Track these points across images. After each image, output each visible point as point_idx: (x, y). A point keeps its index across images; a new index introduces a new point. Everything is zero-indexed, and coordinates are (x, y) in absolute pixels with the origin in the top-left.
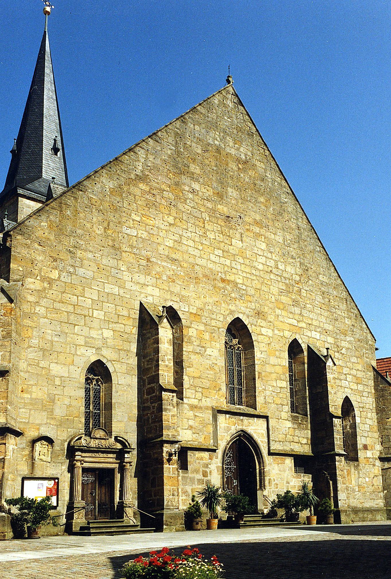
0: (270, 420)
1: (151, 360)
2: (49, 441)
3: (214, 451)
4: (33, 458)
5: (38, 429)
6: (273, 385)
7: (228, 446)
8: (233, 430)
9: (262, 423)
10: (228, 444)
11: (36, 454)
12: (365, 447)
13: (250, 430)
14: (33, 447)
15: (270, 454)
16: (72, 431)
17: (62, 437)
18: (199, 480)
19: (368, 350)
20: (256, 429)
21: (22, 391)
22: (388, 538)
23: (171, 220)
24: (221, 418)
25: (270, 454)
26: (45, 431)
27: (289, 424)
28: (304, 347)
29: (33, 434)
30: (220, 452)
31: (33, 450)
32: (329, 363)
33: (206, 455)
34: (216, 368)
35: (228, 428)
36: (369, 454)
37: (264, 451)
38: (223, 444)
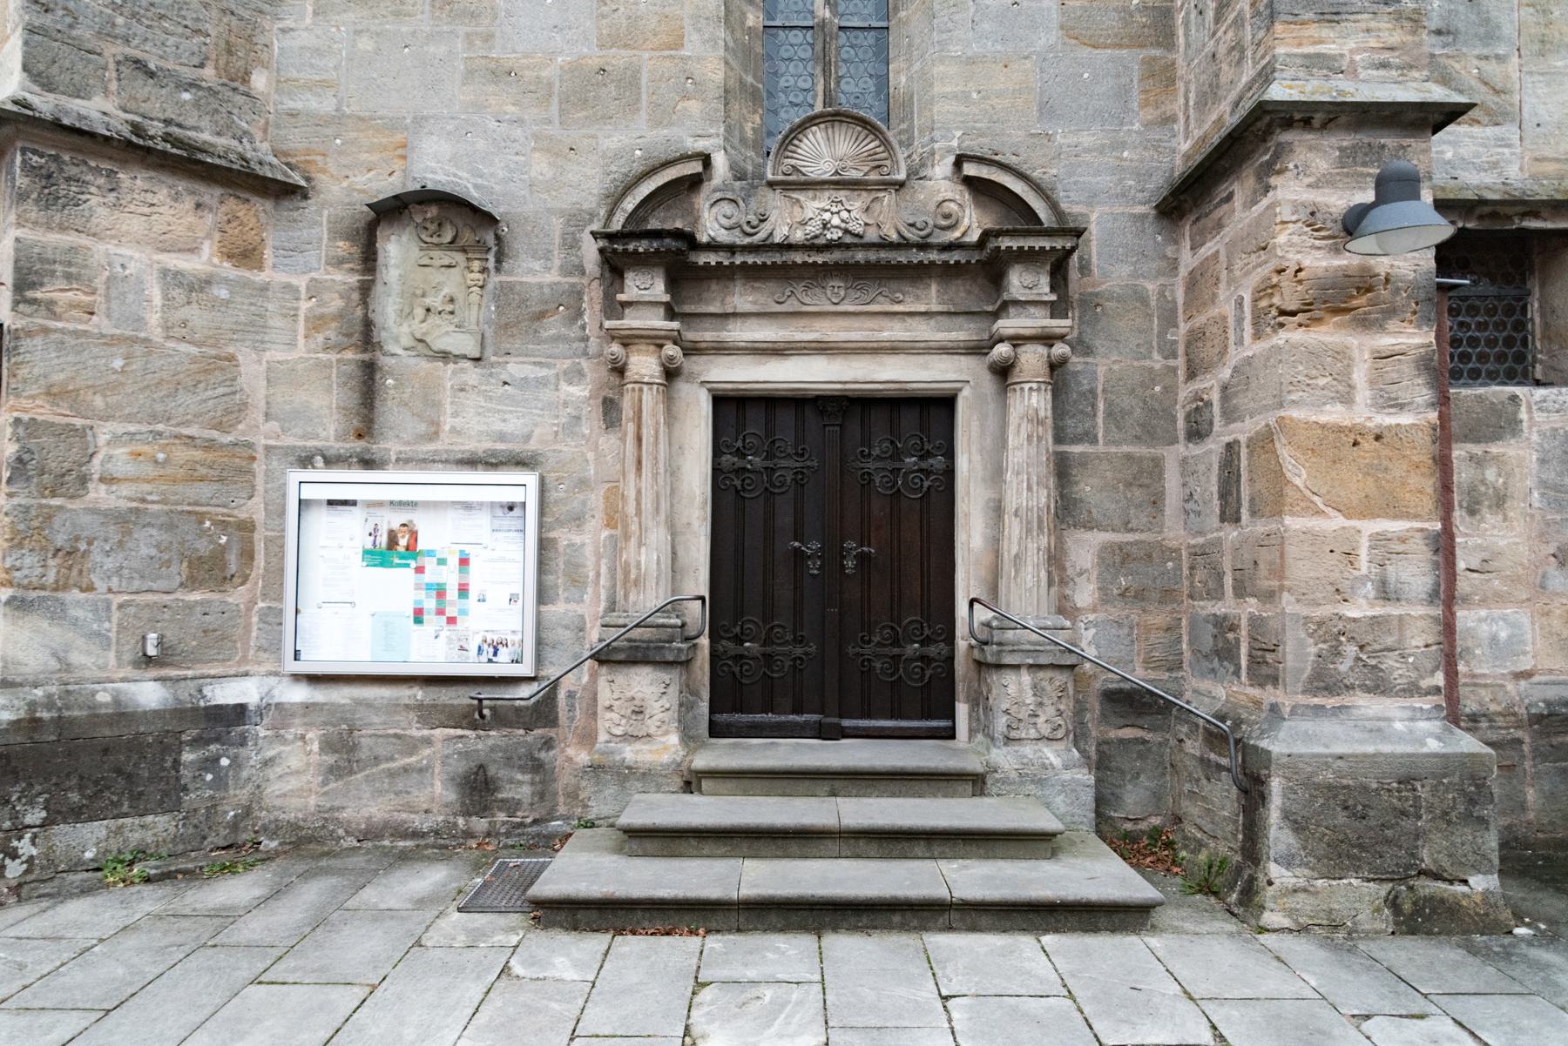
2: (457, 219)
4: (367, 335)
5: (403, 151)
11: (388, 308)
14: (369, 259)
17: (552, 183)
22: (846, 723)
26: (436, 165)
29: (351, 181)
31: (366, 290)
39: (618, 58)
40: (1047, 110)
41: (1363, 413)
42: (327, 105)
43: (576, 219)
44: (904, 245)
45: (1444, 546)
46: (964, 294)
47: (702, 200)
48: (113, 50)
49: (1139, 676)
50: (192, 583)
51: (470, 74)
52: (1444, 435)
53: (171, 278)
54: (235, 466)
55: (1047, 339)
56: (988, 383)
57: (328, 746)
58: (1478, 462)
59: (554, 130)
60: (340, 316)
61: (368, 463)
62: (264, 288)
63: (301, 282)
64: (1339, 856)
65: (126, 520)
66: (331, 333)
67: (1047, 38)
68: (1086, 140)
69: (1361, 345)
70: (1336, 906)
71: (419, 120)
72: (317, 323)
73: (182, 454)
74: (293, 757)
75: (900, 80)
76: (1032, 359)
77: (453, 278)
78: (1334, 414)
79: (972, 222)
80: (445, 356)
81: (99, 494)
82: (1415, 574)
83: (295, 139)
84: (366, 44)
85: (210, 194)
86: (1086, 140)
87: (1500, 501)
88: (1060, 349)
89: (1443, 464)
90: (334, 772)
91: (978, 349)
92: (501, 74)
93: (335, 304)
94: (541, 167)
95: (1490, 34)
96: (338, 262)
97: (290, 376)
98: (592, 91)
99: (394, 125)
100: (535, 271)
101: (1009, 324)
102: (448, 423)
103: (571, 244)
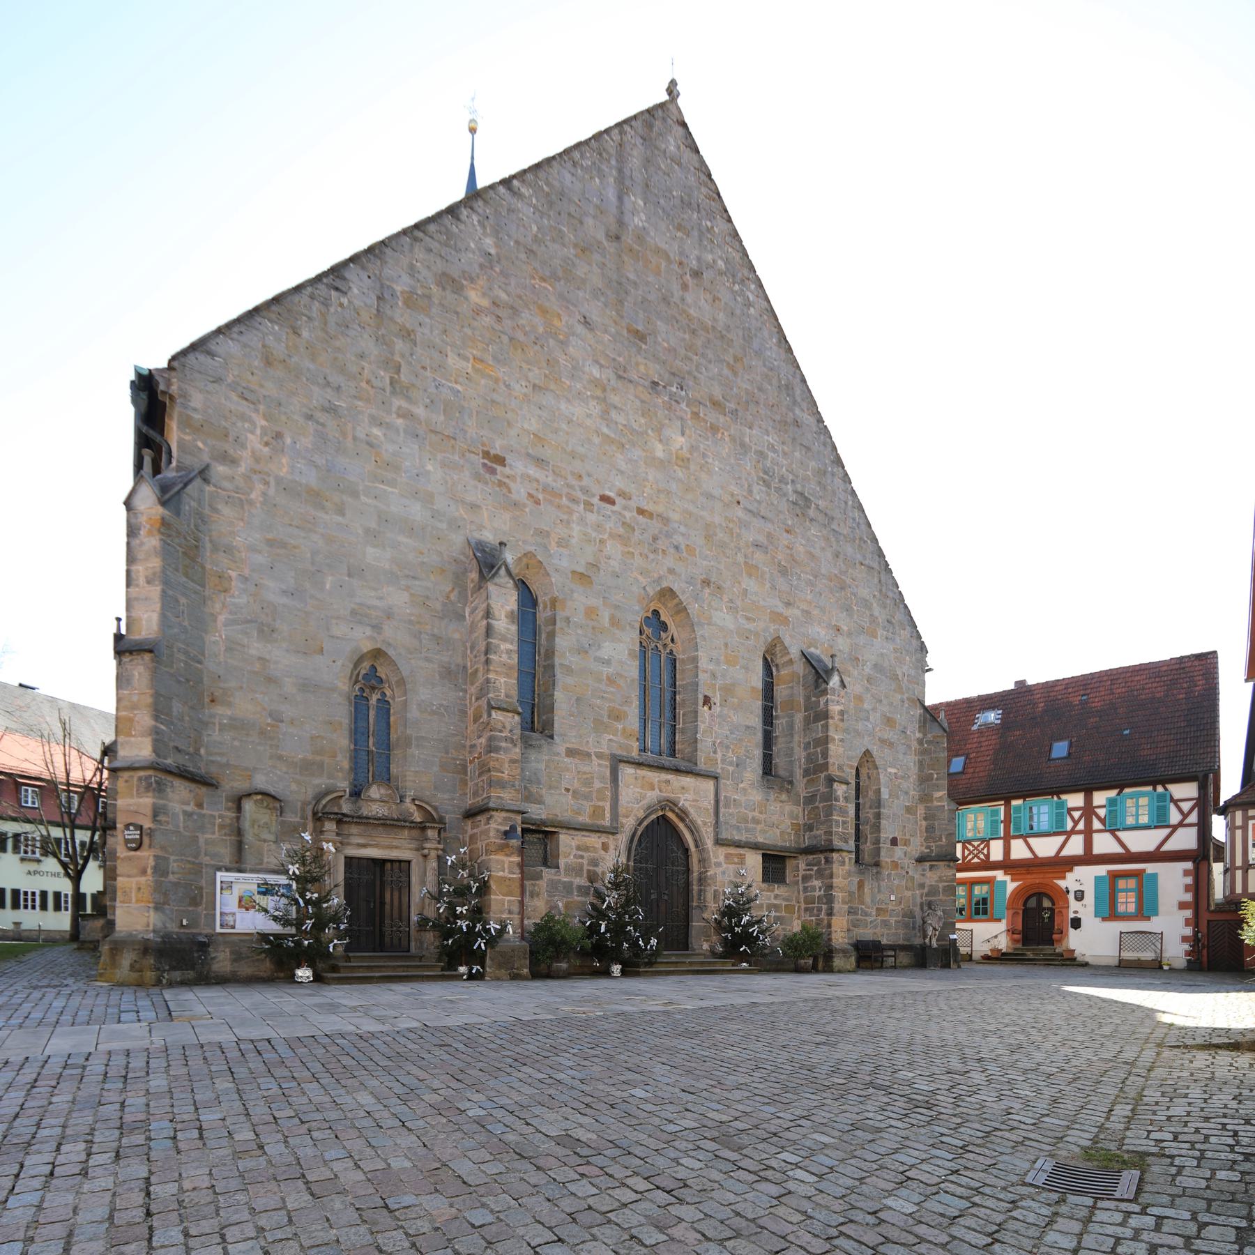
0: (722, 781)
1: (622, 133)
3: (613, 834)
4: (239, 832)
5: (250, 777)
6: (726, 727)
7: (641, 829)
8: (652, 796)
9: (710, 785)
10: (640, 824)
12: (894, 842)
13: (685, 801)
14: (239, 809)
15: (719, 842)
16: (321, 782)
18: (580, 888)
19: (545, 281)
20: (692, 795)
21: (212, 701)
23: (535, 375)
24: (627, 772)
25: (719, 842)
26: (260, 782)
27: (756, 796)
28: (794, 652)
30: (623, 839)
31: (238, 818)
32: (834, 681)
33: (594, 840)
34: (621, 682)
35: (639, 793)
36: (899, 851)
37: (709, 843)
38: (629, 823)
39: (318, 758)
40: (436, 788)
41: (506, 874)
42: (224, 760)
43: (305, 804)
44: (398, 820)
45: (522, 903)
46: (415, 833)
47: (342, 801)
48: (172, 744)
49: (470, 801)
50: (190, 905)
51: (271, 757)
52: (522, 879)
53: (185, 812)
54: (197, 870)
55: (437, 849)
56: (421, 859)
57: (232, 953)
58: (534, 885)
59: (298, 777)
60: (231, 825)
61: (240, 871)
62: (204, 815)
63: (216, 814)
64: (500, 966)
65: (176, 884)
66: (227, 831)
67: (436, 769)
68: (446, 796)
69: (507, 859)
70: (288, 441)
71: (255, 769)
72: (222, 827)
73: (188, 866)
74: (221, 956)
75: (394, 770)
76: (433, 854)
77: (264, 816)
78: (501, 874)
79: (417, 817)
80: (265, 841)
81: (171, 877)
82: (516, 908)
83: (214, 770)
84: (236, 743)
85: (193, 786)
86: (446, 796)
87: (538, 895)
88: (440, 852)
89: (522, 886)
90: (235, 960)
91: (417, 850)
92: (280, 758)
93: (228, 821)
94: (294, 787)
95: (539, 783)
96: (229, 809)
97: (215, 841)
98: (307, 767)
99: (247, 769)
100: (292, 818)
101: (428, 845)
102: (265, 860)
103: (303, 810)
